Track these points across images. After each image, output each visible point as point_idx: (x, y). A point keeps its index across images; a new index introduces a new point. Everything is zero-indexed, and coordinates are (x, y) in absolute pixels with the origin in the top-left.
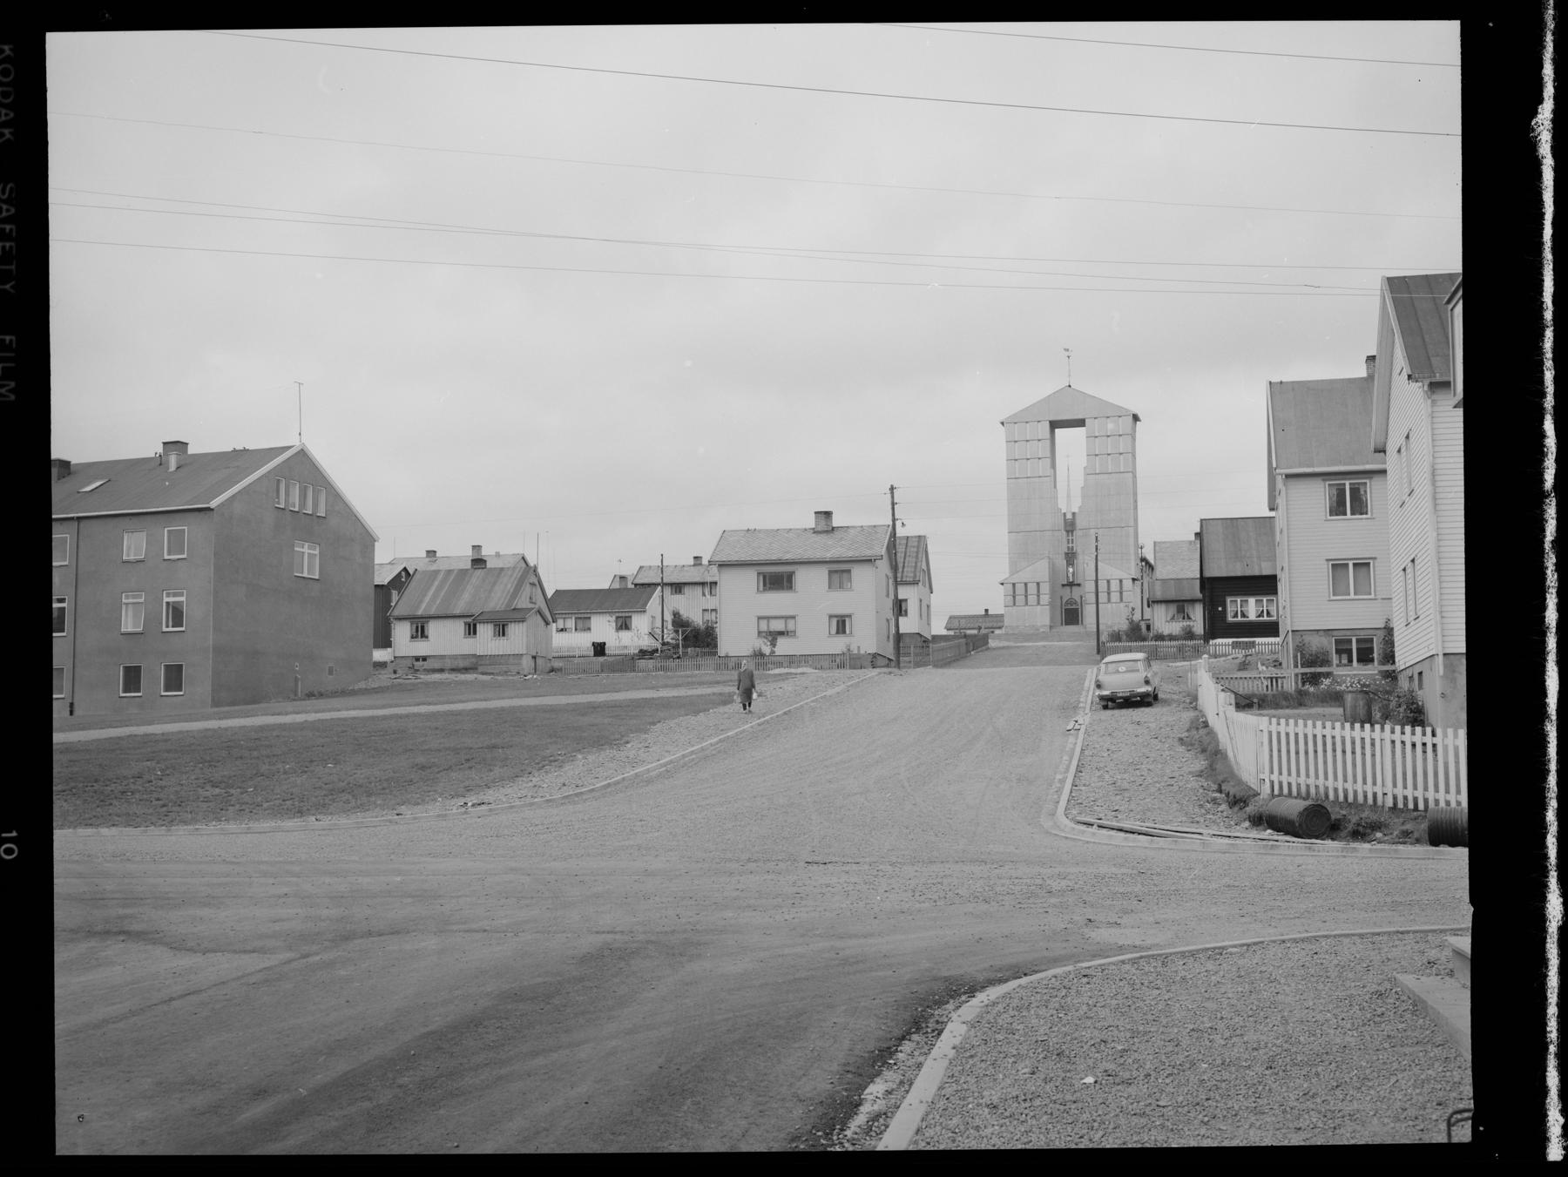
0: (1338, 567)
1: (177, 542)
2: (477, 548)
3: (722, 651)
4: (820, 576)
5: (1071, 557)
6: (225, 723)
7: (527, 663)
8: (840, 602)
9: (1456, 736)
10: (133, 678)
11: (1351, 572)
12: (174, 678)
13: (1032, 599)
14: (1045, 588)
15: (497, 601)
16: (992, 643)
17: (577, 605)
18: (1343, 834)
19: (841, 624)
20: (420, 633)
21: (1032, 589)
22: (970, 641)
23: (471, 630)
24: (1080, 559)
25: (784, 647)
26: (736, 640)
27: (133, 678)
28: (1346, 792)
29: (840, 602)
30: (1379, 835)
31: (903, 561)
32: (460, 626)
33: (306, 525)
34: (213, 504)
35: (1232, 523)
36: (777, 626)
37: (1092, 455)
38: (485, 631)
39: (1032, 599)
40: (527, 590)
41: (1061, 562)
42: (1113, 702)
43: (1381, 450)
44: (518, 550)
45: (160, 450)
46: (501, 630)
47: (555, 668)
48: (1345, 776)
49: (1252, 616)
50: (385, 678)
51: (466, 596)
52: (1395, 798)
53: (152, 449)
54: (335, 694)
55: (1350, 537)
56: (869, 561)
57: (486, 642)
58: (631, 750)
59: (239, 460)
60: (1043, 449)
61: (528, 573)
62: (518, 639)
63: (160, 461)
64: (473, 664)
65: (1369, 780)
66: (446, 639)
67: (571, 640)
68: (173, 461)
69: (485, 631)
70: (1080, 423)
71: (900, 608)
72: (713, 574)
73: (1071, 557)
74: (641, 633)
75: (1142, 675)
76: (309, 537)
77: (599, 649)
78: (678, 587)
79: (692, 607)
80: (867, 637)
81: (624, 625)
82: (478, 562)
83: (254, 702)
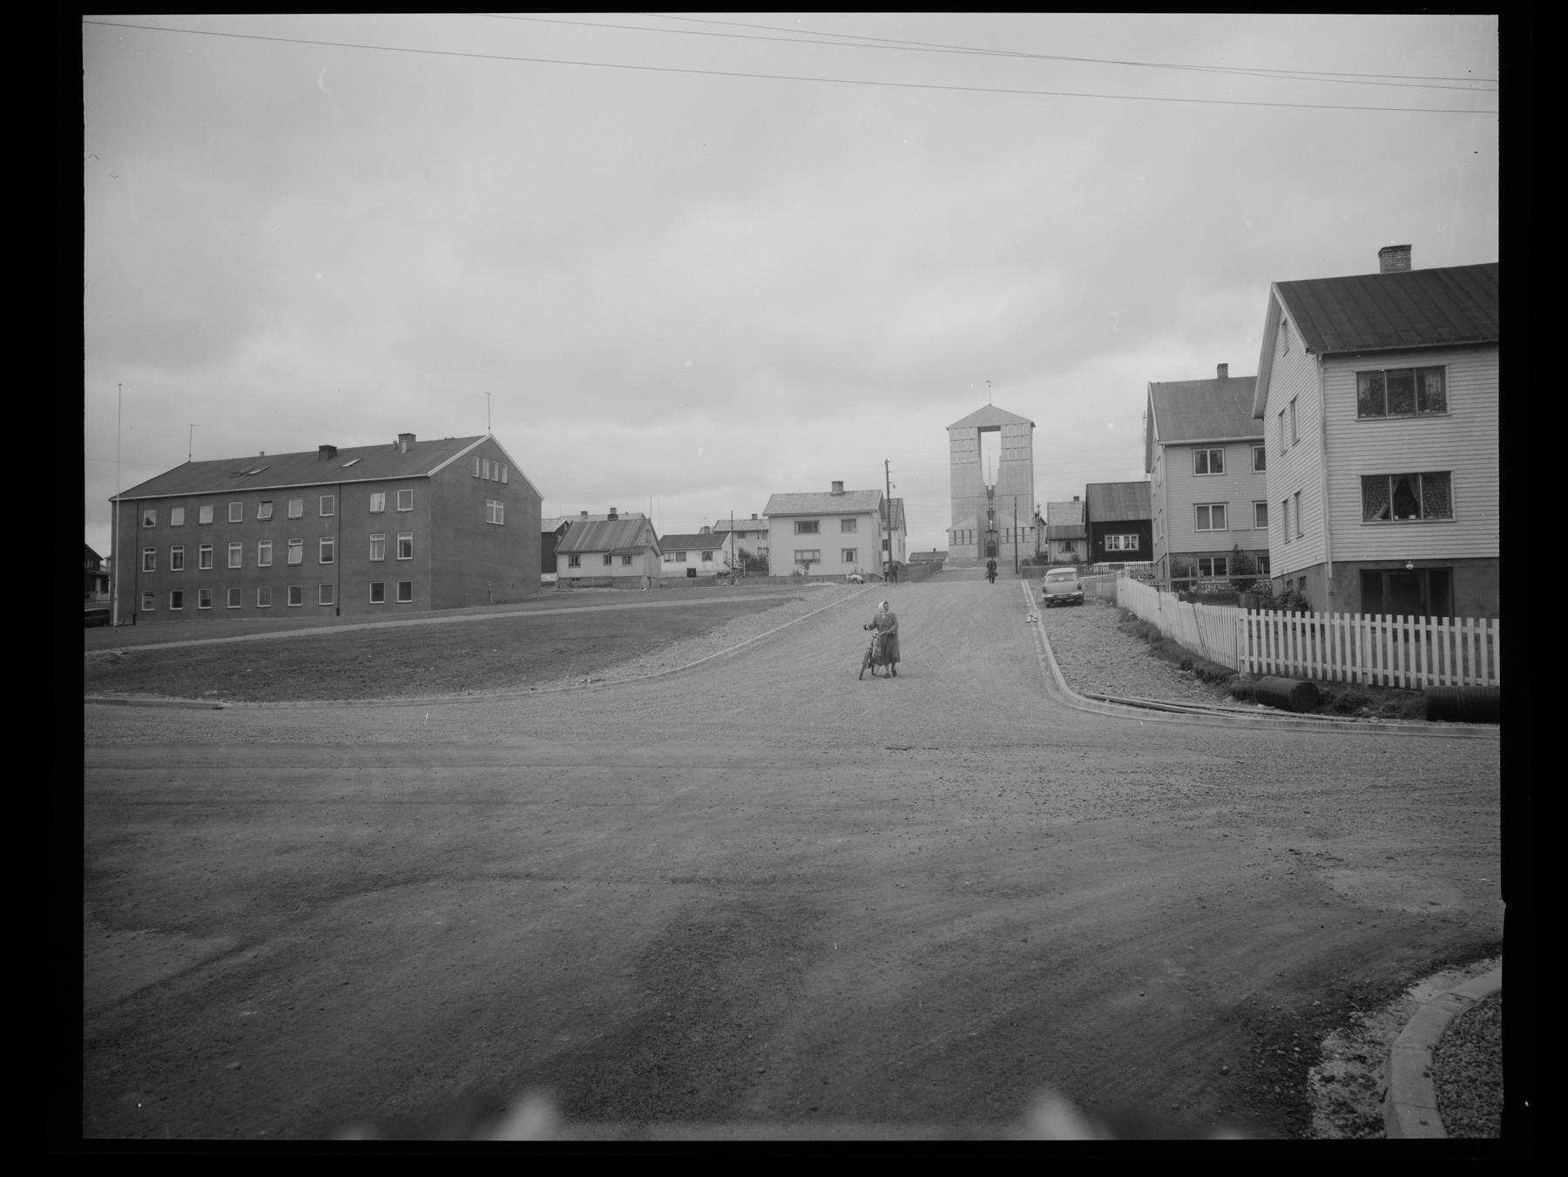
0: (1202, 509)
1: (405, 496)
2: (613, 509)
3: (772, 573)
4: (836, 523)
5: (991, 514)
6: (429, 621)
7: (645, 581)
8: (849, 540)
9: (1489, 625)
10: (378, 592)
11: (1211, 513)
12: (406, 591)
13: (967, 540)
14: (975, 534)
15: (624, 541)
16: (945, 568)
17: (677, 545)
18: (1329, 707)
19: (850, 555)
20: (575, 562)
21: (967, 534)
22: (930, 566)
23: (608, 561)
24: (998, 515)
25: (814, 570)
26: (781, 564)
27: (378, 592)
28: (1334, 672)
29: (849, 540)
30: (1365, 709)
31: (890, 513)
32: (600, 558)
33: (495, 489)
34: (430, 473)
35: (1108, 487)
36: (808, 556)
37: (1004, 449)
38: (617, 561)
39: (967, 540)
40: (644, 535)
41: (985, 516)
42: (1052, 603)
43: (1260, 416)
44: (640, 511)
45: (397, 439)
46: (627, 560)
47: (665, 585)
48: (1334, 658)
49: (1122, 548)
50: (549, 591)
51: (605, 538)
52: (1375, 677)
53: (389, 438)
54: (515, 601)
55: (1210, 488)
56: (868, 513)
57: (618, 568)
58: (714, 638)
59: (450, 445)
60: (973, 445)
61: (644, 523)
62: (638, 566)
63: (396, 446)
64: (610, 582)
65: (1319, 657)
66: (592, 566)
67: (673, 567)
68: (404, 446)
69: (617, 561)
70: (997, 428)
71: (886, 545)
72: (766, 525)
73: (991, 514)
74: (720, 561)
75: (1075, 583)
76: (496, 496)
77: (692, 573)
78: (742, 534)
79: (752, 546)
80: (866, 562)
81: (707, 557)
82: (613, 516)
83: (460, 606)
